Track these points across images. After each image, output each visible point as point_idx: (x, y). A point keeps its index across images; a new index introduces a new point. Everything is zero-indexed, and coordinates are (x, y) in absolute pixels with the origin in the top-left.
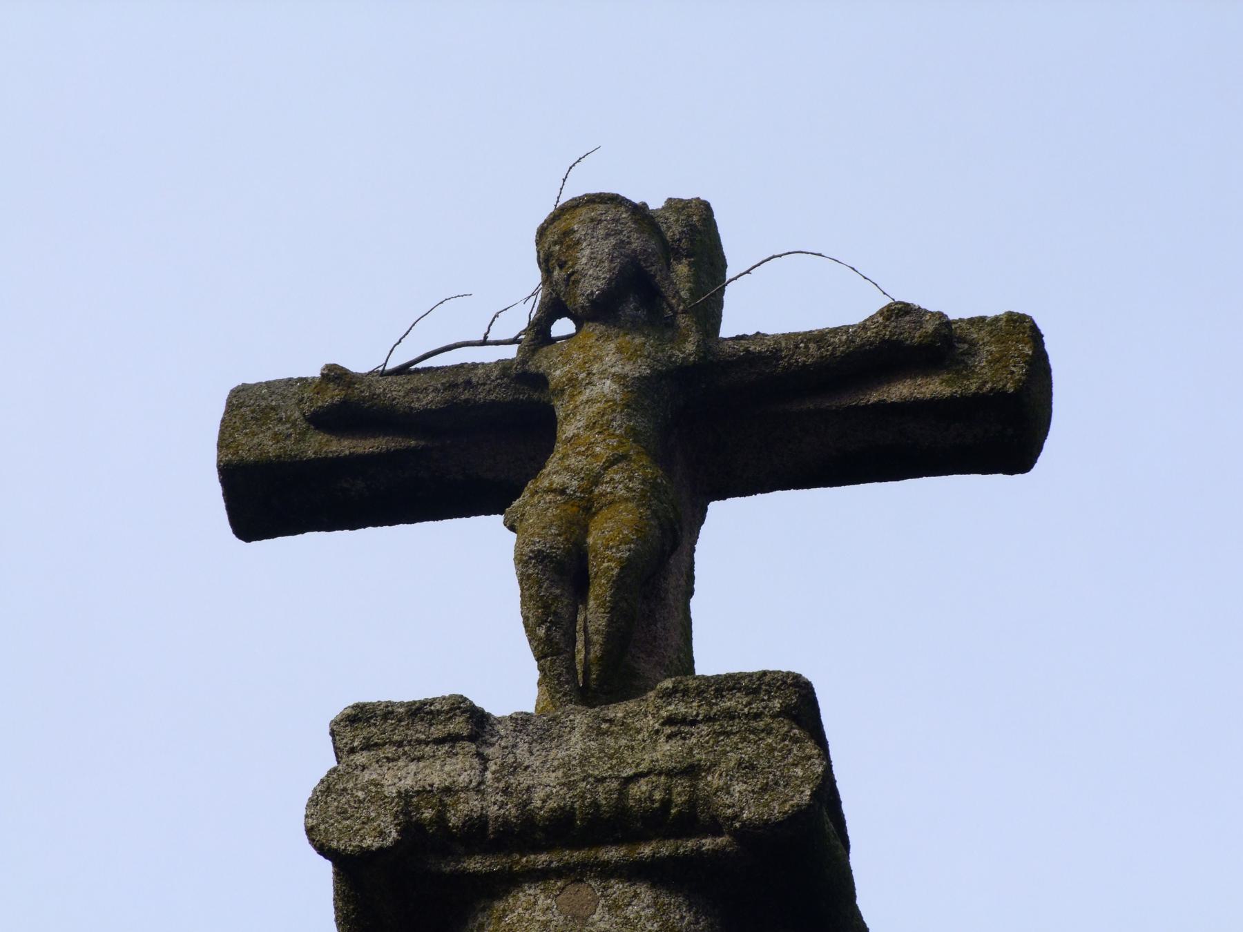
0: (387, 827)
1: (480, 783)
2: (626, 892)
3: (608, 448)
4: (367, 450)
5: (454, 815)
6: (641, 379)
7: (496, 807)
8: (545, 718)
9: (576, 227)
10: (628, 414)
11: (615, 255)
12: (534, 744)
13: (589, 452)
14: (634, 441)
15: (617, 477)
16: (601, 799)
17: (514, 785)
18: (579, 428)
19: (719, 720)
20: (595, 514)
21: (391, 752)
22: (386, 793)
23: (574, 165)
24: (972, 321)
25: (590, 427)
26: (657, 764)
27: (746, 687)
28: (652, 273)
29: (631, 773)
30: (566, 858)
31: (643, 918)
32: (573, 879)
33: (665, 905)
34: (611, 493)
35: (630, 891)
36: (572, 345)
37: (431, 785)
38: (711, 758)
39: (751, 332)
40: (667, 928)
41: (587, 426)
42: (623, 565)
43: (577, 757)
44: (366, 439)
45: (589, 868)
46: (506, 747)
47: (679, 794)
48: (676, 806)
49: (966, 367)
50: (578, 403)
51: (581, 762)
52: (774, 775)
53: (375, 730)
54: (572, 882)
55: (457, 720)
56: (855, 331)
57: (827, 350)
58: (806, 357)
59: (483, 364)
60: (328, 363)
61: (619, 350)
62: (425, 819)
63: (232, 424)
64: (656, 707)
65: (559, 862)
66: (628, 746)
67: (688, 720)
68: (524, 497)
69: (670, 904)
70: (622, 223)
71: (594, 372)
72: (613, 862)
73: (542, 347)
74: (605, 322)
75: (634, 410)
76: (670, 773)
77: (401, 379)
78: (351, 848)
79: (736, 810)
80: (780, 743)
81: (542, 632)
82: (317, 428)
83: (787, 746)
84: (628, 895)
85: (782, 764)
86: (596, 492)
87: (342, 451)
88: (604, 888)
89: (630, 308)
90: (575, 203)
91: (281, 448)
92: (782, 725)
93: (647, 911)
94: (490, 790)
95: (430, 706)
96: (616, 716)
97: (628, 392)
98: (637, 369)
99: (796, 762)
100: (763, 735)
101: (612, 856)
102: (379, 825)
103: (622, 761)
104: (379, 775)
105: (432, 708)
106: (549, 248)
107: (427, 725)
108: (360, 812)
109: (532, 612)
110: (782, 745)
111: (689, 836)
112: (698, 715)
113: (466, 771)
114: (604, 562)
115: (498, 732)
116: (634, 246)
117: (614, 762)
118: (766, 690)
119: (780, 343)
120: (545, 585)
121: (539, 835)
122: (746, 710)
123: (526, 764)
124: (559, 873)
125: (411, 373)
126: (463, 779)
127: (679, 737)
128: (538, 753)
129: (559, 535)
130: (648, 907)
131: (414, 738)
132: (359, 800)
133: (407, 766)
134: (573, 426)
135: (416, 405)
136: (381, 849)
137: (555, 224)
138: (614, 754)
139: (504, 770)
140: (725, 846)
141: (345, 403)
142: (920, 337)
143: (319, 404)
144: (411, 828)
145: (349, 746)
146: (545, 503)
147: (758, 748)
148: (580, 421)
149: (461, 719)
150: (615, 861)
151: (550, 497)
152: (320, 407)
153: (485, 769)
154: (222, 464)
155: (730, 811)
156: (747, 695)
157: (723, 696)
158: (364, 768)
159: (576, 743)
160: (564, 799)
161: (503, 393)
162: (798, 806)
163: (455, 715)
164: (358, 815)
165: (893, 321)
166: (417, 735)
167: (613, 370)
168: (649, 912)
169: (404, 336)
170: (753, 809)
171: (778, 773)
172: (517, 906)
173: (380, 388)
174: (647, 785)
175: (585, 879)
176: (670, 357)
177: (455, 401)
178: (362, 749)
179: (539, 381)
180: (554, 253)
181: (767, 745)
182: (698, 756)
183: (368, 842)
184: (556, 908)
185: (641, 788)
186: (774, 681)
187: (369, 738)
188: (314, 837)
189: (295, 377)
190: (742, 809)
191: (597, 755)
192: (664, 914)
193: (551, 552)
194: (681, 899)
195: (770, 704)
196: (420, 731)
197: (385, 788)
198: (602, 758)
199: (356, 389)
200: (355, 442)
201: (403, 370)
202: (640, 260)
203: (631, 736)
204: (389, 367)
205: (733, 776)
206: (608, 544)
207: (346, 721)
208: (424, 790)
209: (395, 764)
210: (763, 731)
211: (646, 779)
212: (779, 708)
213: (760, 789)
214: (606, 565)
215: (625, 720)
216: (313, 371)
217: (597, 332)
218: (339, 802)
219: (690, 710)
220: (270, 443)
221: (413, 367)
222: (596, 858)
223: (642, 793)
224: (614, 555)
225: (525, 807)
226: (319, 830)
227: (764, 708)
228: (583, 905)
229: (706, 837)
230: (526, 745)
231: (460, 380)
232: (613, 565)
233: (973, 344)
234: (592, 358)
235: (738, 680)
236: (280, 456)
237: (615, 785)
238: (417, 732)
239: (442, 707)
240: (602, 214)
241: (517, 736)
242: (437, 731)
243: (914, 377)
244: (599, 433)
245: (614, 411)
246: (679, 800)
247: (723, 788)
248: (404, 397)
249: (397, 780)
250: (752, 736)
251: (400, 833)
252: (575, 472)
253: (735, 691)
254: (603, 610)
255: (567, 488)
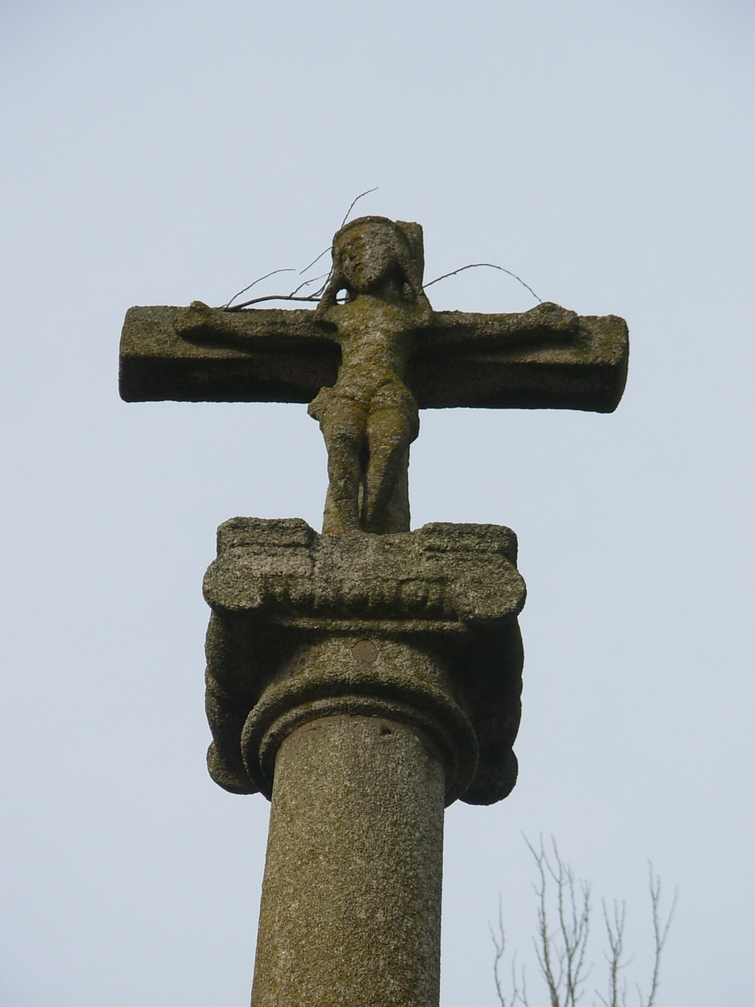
0: (255, 595)
1: (312, 574)
2: (395, 649)
3: (380, 375)
4: (214, 356)
5: (295, 592)
6: (398, 333)
7: (321, 590)
8: (350, 538)
9: (362, 236)
10: (390, 354)
11: (385, 255)
12: (344, 554)
13: (369, 376)
14: (394, 371)
15: (386, 393)
16: (386, 592)
17: (332, 578)
18: (361, 360)
19: (460, 551)
20: (371, 414)
21: (257, 549)
22: (254, 574)
23: (359, 197)
24: (588, 318)
25: (368, 360)
26: (421, 574)
27: (478, 533)
28: (405, 269)
29: (405, 578)
30: (360, 625)
31: (405, 666)
32: (363, 638)
33: (417, 660)
34: (382, 402)
35: (397, 649)
36: (354, 307)
37: (281, 572)
38: (454, 574)
39: (452, 310)
40: (419, 674)
41: (366, 359)
42: (394, 448)
43: (371, 565)
44: (214, 349)
45: (373, 633)
46: (327, 554)
47: (433, 594)
48: (431, 601)
49: (586, 346)
50: (359, 344)
51: (373, 568)
52: (494, 589)
53: (248, 535)
54: (362, 640)
55: (298, 534)
56: (522, 318)
57: (505, 327)
58: (492, 329)
59: (286, 311)
60: (195, 300)
61: (385, 314)
62: (277, 593)
63: (130, 330)
64: (421, 539)
65: (355, 627)
66: (403, 561)
67: (441, 549)
68: (320, 397)
69: (420, 659)
70: (390, 237)
71: (370, 326)
72: (388, 630)
73: (332, 306)
74: (375, 295)
75: (394, 352)
76: (429, 581)
77: (239, 314)
78: (232, 606)
79: (472, 608)
80: (497, 569)
81: (341, 483)
82: (183, 339)
83: (501, 572)
84: (395, 651)
85: (499, 582)
86: (373, 400)
87: (199, 355)
88: (381, 645)
89: (390, 288)
90: (362, 221)
91: (161, 349)
92: (498, 558)
93: (407, 662)
94: (317, 579)
95: (283, 523)
96: (394, 542)
97: (390, 341)
98: (396, 327)
99: (507, 582)
100: (486, 563)
101: (388, 627)
102: (250, 594)
103: (399, 570)
104: (249, 562)
105: (284, 525)
106: (344, 247)
107: (279, 535)
108: (238, 584)
109: (336, 471)
110: (498, 571)
111: (436, 619)
112: (447, 547)
113: (302, 566)
114: (381, 445)
115: (321, 544)
116: (396, 251)
117: (394, 570)
118: (490, 536)
119: (477, 320)
120: (345, 455)
121: (345, 610)
122: (477, 547)
123: (339, 565)
124: (354, 634)
125: (241, 311)
126: (301, 570)
127: (434, 559)
128: (346, 559)
129: (354, 425)
130: (407, 660)
131: (271, 542)
132: (237, 577)
133: (266, 559)
134: (357, 358)
135: (250, 332)
136: (251, 608)
137: (348, 232)
138: (394, 565)
139: (325, 567)
140: (458, 628)
141: (204, 326)
142: (561, 325)
143: (189, 325)
144: (269, 598)
145: (231, 543)
146: (341, 404)
147: (484, 571)
148: (361, 355)
149: (301, 534)
150: (390, 631)
151: (344, 400)
152: (189, 327)
153: (314, 566)
154: (124, 354)
155: (467, 608)
156: (478, 538)
157: (463, 537)
158: (239, 557)
159: (370, 556)
160: (363, 589)
161: (306, 331)
162: (509, 609)
163: (298, 531)
164: (237, 586)
165: (545, 314)
166: (273, 541)
167: (382, 326)
168: (408, 663)
169: (245, 290)
170: (481, 608)
171: (496, 588)
172: (327, 651)
173: (227, 320)
174: (414, 586)
175: (370, 639)
176: (413, 322)
177: (274, 333)
178: (238, 545)
179: (332, 327)
180: (347, 250)
181: (489, 569)
182: (446, 572)
183: (243, 603)
184: (352, 655)
185: (409, 588)
186: (495, 532)
187: (243, 540)
188: (210, 597)
189: (169, 306)
190: (475, 607)
191: (383, 564)
192: (416, 665)
193: (351, 436)
194: (426, 657)
195: (492, 545)
196: (275, 538)
197: (253, 571)
198: (387, 567)
199: (212, 318)
200: (207, 350)
201: (237, 309)
202: (399, 260)
203: (404, 555)
204: (230, 306)
205: (468, 587)
206: (385, 435)
207: (230, 527)
208: (277, 575)
209: (258, 556)
210: (486, 561)
211: (414, 582)
212: (498, 548)
213: (485, 596)
214: (383, 447)
215: (400, 545)
216: (185, 303)
217: (370, 301)
218: (224, 576)
219: (443, 543)
220: (154, 345)
221: (243, 308)
222: (378, 627)
223: (411, 591)
224: (388, 441)
225: (338, 591)
226: (213, 593)
227: (488, 547)
228: (368, 655)
229: (446, 622)
230: (339, 553)
231: (279, 320)
232: (388, 448)
233: (590, 333)
234: (368, 317)
235: (473, 528)
236: (160, 354)
237: (394, 584)
238: (274, 538)
239: (290, 525)
240: (378, 230)
241: (333, 548)
242: (286, 540)
243: (554, 349)
244: (374, 364)
245: (382, 352)
246: (433, 598)
247: (463, 594)
248: (243, 327)
249: (260, 567)
250: (479, 563)
251: (262, 600)
252: (360, 387)
253: (470, 535)
254: (379, 474)
255: (355, 396)
